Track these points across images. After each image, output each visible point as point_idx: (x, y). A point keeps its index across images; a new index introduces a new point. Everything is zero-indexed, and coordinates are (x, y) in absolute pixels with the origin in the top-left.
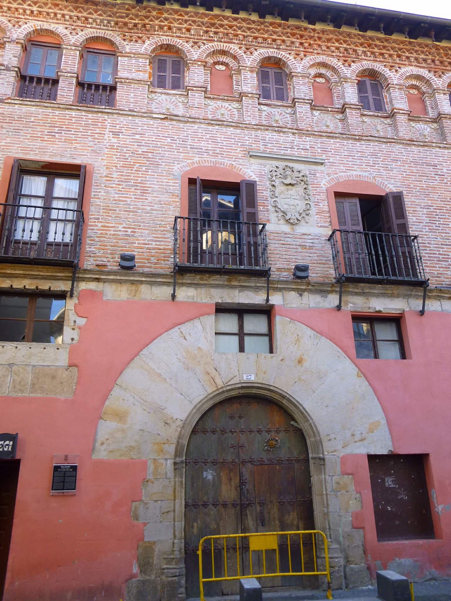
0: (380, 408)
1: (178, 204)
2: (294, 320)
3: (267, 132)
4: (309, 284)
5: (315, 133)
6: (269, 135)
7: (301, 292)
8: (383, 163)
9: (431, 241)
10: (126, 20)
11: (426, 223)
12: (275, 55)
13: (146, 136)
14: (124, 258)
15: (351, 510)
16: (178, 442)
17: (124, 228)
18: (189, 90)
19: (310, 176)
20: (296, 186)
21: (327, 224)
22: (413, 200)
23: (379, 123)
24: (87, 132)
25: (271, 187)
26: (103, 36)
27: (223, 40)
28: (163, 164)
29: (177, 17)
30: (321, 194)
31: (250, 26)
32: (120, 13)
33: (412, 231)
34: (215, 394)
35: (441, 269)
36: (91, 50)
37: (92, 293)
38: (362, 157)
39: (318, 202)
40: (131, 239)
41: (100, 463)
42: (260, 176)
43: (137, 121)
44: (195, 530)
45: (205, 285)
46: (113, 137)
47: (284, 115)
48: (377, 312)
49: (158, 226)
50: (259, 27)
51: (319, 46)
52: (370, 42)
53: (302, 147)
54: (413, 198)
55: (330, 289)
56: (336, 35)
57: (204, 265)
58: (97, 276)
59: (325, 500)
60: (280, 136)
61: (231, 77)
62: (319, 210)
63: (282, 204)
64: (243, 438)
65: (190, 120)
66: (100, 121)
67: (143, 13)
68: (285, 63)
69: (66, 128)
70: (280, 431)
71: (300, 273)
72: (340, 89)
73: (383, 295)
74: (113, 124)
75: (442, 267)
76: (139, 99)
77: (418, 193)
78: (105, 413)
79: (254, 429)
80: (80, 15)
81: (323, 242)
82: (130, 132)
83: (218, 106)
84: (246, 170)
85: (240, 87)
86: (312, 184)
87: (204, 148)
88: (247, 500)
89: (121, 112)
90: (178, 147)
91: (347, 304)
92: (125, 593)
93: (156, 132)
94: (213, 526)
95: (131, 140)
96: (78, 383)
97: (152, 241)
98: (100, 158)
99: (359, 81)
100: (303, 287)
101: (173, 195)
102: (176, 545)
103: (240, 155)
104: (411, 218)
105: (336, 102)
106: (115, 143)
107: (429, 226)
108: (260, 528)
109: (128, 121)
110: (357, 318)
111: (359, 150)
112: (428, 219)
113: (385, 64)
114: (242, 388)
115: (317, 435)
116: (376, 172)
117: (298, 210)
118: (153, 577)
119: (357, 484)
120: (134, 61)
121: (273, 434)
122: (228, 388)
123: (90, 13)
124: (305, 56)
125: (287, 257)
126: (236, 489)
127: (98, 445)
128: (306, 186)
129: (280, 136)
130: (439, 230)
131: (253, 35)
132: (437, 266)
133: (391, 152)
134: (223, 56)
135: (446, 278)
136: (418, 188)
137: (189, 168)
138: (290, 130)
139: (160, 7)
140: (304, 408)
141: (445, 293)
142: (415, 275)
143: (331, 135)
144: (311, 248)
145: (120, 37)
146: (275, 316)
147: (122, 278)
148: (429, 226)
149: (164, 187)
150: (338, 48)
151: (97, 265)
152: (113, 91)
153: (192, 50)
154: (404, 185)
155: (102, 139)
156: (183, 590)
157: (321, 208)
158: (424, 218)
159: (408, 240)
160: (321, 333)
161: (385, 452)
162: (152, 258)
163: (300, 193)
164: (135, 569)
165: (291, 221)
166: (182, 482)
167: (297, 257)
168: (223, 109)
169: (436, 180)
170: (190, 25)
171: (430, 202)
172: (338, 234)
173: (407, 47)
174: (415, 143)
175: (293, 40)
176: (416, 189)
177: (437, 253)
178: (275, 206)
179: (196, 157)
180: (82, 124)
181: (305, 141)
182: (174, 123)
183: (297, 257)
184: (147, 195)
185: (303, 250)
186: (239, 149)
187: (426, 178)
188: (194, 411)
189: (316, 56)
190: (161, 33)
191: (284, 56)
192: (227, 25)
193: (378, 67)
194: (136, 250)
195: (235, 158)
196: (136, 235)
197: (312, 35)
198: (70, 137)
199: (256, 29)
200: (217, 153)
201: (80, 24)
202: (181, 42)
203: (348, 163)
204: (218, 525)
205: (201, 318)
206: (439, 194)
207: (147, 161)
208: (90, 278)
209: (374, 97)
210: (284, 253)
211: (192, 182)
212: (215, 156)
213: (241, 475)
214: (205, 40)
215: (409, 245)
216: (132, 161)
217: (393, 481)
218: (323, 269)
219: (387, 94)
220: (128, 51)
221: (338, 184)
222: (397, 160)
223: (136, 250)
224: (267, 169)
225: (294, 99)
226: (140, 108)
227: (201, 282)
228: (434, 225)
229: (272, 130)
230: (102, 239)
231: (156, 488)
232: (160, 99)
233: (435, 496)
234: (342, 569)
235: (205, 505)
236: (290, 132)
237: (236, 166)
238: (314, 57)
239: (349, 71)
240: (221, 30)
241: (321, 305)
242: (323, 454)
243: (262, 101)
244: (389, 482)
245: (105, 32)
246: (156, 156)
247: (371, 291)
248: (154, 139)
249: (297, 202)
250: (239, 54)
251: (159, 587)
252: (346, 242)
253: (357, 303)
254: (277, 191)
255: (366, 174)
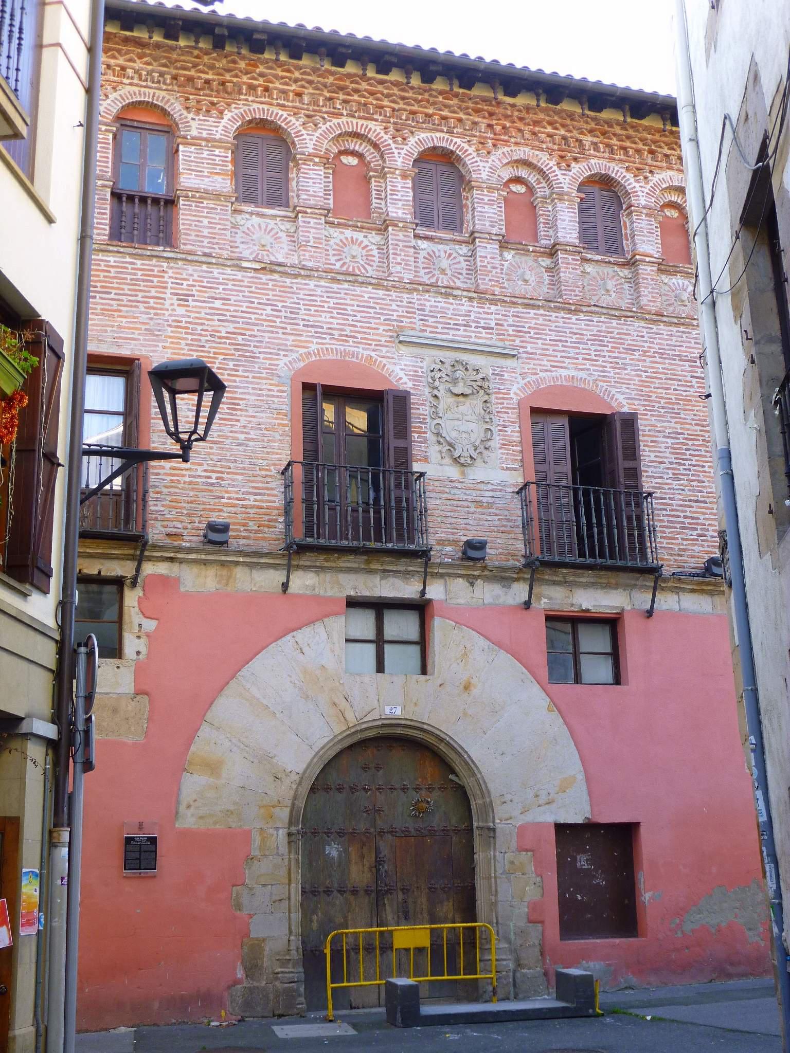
0: (577, 756)
1: (287, 429)
2: (461, 624)
3: (427, 296)
4: (485, 568)
5: (506, 299)
6: (431, 301)
7: (471, 581)
8: (611, 354)
9: (674, 494)
10: (192, 73)
11: (670, 463)
12: (444, 145)
13: (232, 302)
14: (212, 527)
15: (527, 899)
16: (293, 804)
17: (206, 471)
18: (299, 212)
19: (493, 377)
20: (471, 397)
21: (517, 465)
22: (654, 423)
23: (610, 276)
24: (136, 296)
25: (432, 399)
26: (150, 100)
27: (356, 115)
28: (262, 356)
29: (281, 74)
30: (510, 411)
31: (406, 94)
32: (184, 61)
33: (647, 485)
34: (345, 734)
35: (685, 543)
36: (128, 123)
37: (164, 580)
38: (579, 343)
39: (504, 426)
40: (217, 491)
41: (185, 834)
42: (415, 378)
43: (216, 275)
44: (315, 926)
45: (331, 568)
46: (179, 305)
47: (455, 258)
48: (583, 611)
49: (258, 468)
50: (420, 97)
51: (520, 130)
52: (606, 128)
53: (482, 325)
54: (653, 419)
55: (515, 576)
56: (549, 115)
57: (333, 541)
58: (172, 555)
59: (493, 885)
60: (449, 303)
61: (368, 180)
62: (506, 440)
63: (450, 433)
64: (381, 798)
65: (302, 272)
66: (155, 273)
67: (223, 63)
68: (459, 159)
69: (102, 287)
70: (434, 789)
71: (473, 552)
72: (550, 208)
73: (594, 585)
74: (176, 278)
75: (687, 539)
76: (216, 231)
77: (662, 411)
78: (190, 763)
79: (397, 786)
80: (112, 62)
81: (509, 495)
82: (206, 295)
83: (347, 238)
84: (392, 368)
85: (383, 202)
86: (496, 393)
87: (325, 326)
88: (386, 885)
89: (190, 257)
90: (285, 323)
91: (539, 599)
92: (228, 1003)
93: (247, 294)
94: (339, 919)
95: (208, 311)
96: (150, 719)
97: (250, 493)
98: (160, 344)
99: (582, 199)
100: (475, 573)
101: (278, 414)
102: (292, 943)
103: (383, 339)
104: (647, 454)
105: (542, 233)
106: (183, 316)
107: (673, 469)
108: (404, 921)
109: (201, 274)
110: (552, 619)
111: (574, 330)
112: (674, 456)
113: (627, 164)
114: (383, 726)
115: (486, 795)
116: (598, 371)
117: (473, 440)
118: (263, 984)
119: (538, 863)
120: (205, 154)
121: (423, 792)
122: (364, 726)
123: (130, 60)
124: (494, 145)
125: (453, 521)
126: (371, 871)
127: (182, 808)
128: (486, 398)
129: (449, 303)
130: (688, 475)
131: (409, 108)
132: (680, 536)
133: (625, 334)
134: (355, 140)
135: (692, 557)
136: (663, 401)
137: (302, 364)
138: (465, 293)
139: (255, 56)
140: (469, 757)
141: (687, 584)
142: (643, 555)
143: (532, 302)
144: (490, 505)
145: (181, 104)
146: (433, 617)
147: (209, 557)
148: (673, 469)
149: (264, 398)
150: (550, 136)
151: (168, 535)
152: (169, 206)
153: (304, 132)
154: (642, 395)
155: (161, 309)
156: (302, 999)
157: (508, 436)
158: (668, 455)
159: (639, 497)
160: (500, 645)
161: (579, 820)
162: (251, 523)
163: (477, 411)
164: (240, 974)
165: (462, 460)
166: (297, 860)
167: (468, 521)
168: (355, 247)
169: (692, 387)
170: (303, 87)
171: (679, 426)
172: (533, 487)
173: (666, 139)
174: (664, 319)
175: (477, 119)
176: (659, 402)
177: (682, 515)
178: (438, 434)
179: (313, 342)
180: (126, 279)
181: (488, 313)
182: (276, 276)
183: (468, 521)
184: (239, 413)
185: (478, 510)
186: (382, 328)
187: (676, 383)
188: (315, 760)
189: (513, 148)
190: (250, 98)
191: (459, 146)
192: (366, 90)
193: (617, 170)
194: (225, 509)
195: (376, 345)
196: (225, 483)
197: (509, 113)
198: (109, 305)
199: (415, 100)
200: (347, 336)
201: (112, 78)
202: (285, 114)
203: (556, 353)
204: (346, 919)
205: (326, 620)
206: (695, 412)
207: (235, 349)
208: (161, 557)
209: (606, 224)
210: (449, 514)
211: (308, 387)
212: (343, 341)
213: (377, 851)
214: (326, 113)
215: (639, 505)
216: (212, 350)
217: (587, 860)
218: (507, 544)
219: (626, 220)
220: (194, 133)
221: (538, 393)
222: (634, 350)
223: (225, 509)
224: (426, 365)
225: (473, 233)
226: (220, 249)
227: (326, 564)
228: (681, 467)
229: (436, 292)
230: (172, 490)
231: (263, 867)
232: (249, 224)
233: (642, 880)
234: (511, 974)
235: (328, 892)
236: (465, 297)
237: (376, 360)
238: (509, 149)
239: (567, 177)
240: (356, 97)
241: (501, 601)
242: (493, 822)
243: (421, 231)
244: (583, 861)
245: (154, 94)
246: (249, 341)
247: (577, 579)
248: (244, 309)
249: (472, 426)
250: (382, 142)
251: (271, 997)
252: (544, 504)
253: (558, 597)
254: (441, 406)
255: (583, 375)
